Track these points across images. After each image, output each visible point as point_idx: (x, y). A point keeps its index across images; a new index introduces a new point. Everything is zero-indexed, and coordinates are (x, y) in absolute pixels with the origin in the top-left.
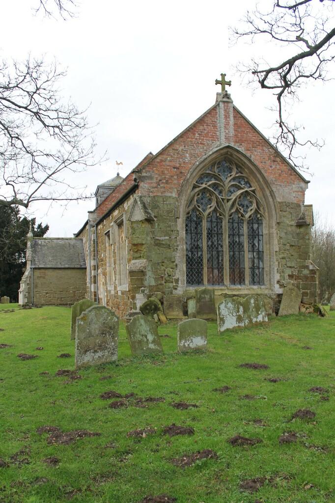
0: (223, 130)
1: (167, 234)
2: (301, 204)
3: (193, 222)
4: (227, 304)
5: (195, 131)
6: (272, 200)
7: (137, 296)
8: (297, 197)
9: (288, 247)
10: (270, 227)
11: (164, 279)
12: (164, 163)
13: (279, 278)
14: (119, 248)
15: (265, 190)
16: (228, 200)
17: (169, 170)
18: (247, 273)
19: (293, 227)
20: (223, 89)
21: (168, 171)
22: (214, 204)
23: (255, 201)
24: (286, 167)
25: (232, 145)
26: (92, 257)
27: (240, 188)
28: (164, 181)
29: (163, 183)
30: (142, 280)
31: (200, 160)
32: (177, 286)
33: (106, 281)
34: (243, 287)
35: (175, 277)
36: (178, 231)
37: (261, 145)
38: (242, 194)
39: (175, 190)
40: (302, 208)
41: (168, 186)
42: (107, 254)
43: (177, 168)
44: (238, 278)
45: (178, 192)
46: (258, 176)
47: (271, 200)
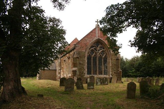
0: (97, 34)
3: (89, 58)
7: (75, 77)
9: (114, 65)
10: (109, 60)
11: (82, 74)
14: (68, 64)
16: (98, 53)
18: (103, 72)
20: (98, 23)
22: (94, 54)
23: (105, 53)
26: (59, 67)
27: (101, 49)
30: (76, 73)
31: (91, 42)
33: (63, 73)
34: (102, 75)
38: (102, 51)
42: (64, 66)
44: (101, 73)
47: (109, 52)
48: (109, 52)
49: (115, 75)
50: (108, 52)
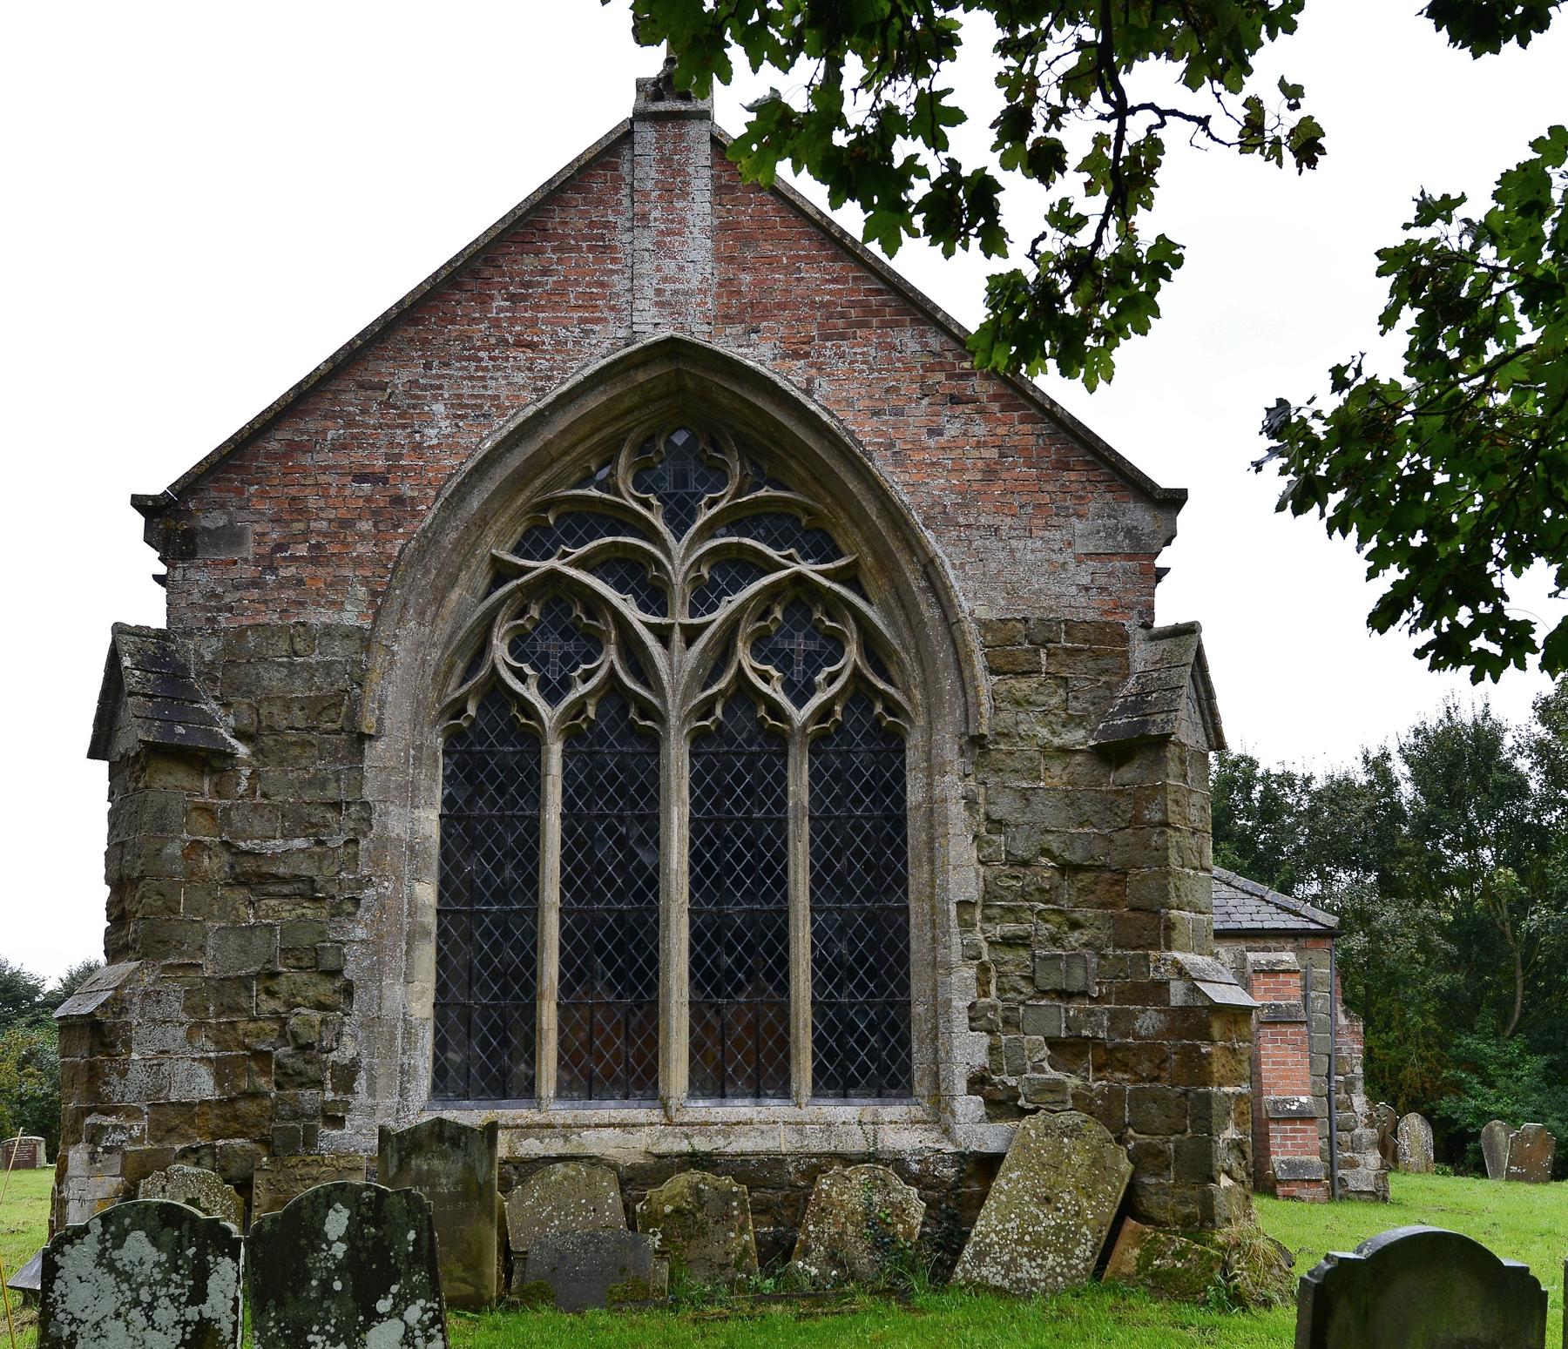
1: (299, 823)
2: (1131, 624)
4: (118, 1245)
5: (487, 281)
6: (937, 613)
8: (1102, 589)
10: (933, 769)
12: (306, 460)
13: (981, 1059)
15: (897, 563)
17: (333, 491)
19: (1079, 758)
21: (326, 497)
23: (851, 632)
24: (1027, 428)
25: (698, 332)
28: (302, 551)
29: (293, 558)
32: (347, 1107)
34: (774, 1109)
35: (333, 1056)
36: (366, 805)
37: (875, 322)
39: (362, 591)
40: (1141, 654)
41: (321, 572)
43: (378, 479)
45: (372, 603)
46: (853, 486)
47: (930, 613)
48: (930, 613)
49: (1082, 1101)
50: (903, 600)
